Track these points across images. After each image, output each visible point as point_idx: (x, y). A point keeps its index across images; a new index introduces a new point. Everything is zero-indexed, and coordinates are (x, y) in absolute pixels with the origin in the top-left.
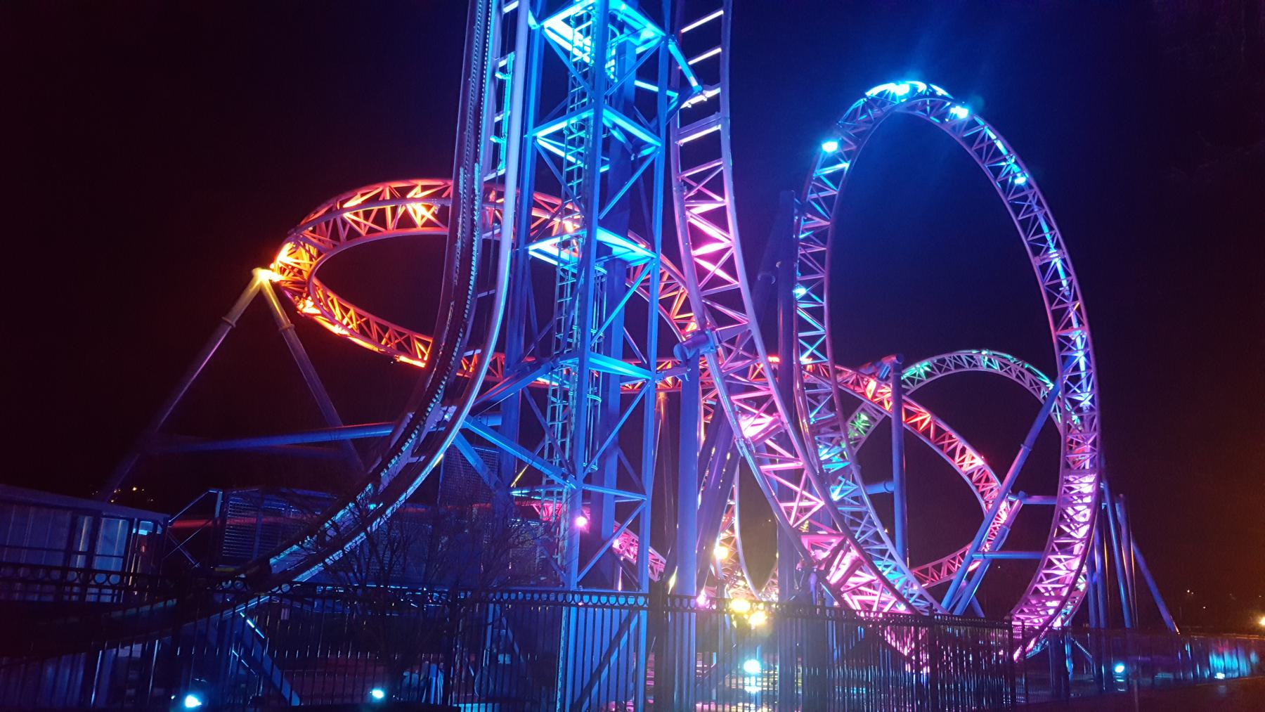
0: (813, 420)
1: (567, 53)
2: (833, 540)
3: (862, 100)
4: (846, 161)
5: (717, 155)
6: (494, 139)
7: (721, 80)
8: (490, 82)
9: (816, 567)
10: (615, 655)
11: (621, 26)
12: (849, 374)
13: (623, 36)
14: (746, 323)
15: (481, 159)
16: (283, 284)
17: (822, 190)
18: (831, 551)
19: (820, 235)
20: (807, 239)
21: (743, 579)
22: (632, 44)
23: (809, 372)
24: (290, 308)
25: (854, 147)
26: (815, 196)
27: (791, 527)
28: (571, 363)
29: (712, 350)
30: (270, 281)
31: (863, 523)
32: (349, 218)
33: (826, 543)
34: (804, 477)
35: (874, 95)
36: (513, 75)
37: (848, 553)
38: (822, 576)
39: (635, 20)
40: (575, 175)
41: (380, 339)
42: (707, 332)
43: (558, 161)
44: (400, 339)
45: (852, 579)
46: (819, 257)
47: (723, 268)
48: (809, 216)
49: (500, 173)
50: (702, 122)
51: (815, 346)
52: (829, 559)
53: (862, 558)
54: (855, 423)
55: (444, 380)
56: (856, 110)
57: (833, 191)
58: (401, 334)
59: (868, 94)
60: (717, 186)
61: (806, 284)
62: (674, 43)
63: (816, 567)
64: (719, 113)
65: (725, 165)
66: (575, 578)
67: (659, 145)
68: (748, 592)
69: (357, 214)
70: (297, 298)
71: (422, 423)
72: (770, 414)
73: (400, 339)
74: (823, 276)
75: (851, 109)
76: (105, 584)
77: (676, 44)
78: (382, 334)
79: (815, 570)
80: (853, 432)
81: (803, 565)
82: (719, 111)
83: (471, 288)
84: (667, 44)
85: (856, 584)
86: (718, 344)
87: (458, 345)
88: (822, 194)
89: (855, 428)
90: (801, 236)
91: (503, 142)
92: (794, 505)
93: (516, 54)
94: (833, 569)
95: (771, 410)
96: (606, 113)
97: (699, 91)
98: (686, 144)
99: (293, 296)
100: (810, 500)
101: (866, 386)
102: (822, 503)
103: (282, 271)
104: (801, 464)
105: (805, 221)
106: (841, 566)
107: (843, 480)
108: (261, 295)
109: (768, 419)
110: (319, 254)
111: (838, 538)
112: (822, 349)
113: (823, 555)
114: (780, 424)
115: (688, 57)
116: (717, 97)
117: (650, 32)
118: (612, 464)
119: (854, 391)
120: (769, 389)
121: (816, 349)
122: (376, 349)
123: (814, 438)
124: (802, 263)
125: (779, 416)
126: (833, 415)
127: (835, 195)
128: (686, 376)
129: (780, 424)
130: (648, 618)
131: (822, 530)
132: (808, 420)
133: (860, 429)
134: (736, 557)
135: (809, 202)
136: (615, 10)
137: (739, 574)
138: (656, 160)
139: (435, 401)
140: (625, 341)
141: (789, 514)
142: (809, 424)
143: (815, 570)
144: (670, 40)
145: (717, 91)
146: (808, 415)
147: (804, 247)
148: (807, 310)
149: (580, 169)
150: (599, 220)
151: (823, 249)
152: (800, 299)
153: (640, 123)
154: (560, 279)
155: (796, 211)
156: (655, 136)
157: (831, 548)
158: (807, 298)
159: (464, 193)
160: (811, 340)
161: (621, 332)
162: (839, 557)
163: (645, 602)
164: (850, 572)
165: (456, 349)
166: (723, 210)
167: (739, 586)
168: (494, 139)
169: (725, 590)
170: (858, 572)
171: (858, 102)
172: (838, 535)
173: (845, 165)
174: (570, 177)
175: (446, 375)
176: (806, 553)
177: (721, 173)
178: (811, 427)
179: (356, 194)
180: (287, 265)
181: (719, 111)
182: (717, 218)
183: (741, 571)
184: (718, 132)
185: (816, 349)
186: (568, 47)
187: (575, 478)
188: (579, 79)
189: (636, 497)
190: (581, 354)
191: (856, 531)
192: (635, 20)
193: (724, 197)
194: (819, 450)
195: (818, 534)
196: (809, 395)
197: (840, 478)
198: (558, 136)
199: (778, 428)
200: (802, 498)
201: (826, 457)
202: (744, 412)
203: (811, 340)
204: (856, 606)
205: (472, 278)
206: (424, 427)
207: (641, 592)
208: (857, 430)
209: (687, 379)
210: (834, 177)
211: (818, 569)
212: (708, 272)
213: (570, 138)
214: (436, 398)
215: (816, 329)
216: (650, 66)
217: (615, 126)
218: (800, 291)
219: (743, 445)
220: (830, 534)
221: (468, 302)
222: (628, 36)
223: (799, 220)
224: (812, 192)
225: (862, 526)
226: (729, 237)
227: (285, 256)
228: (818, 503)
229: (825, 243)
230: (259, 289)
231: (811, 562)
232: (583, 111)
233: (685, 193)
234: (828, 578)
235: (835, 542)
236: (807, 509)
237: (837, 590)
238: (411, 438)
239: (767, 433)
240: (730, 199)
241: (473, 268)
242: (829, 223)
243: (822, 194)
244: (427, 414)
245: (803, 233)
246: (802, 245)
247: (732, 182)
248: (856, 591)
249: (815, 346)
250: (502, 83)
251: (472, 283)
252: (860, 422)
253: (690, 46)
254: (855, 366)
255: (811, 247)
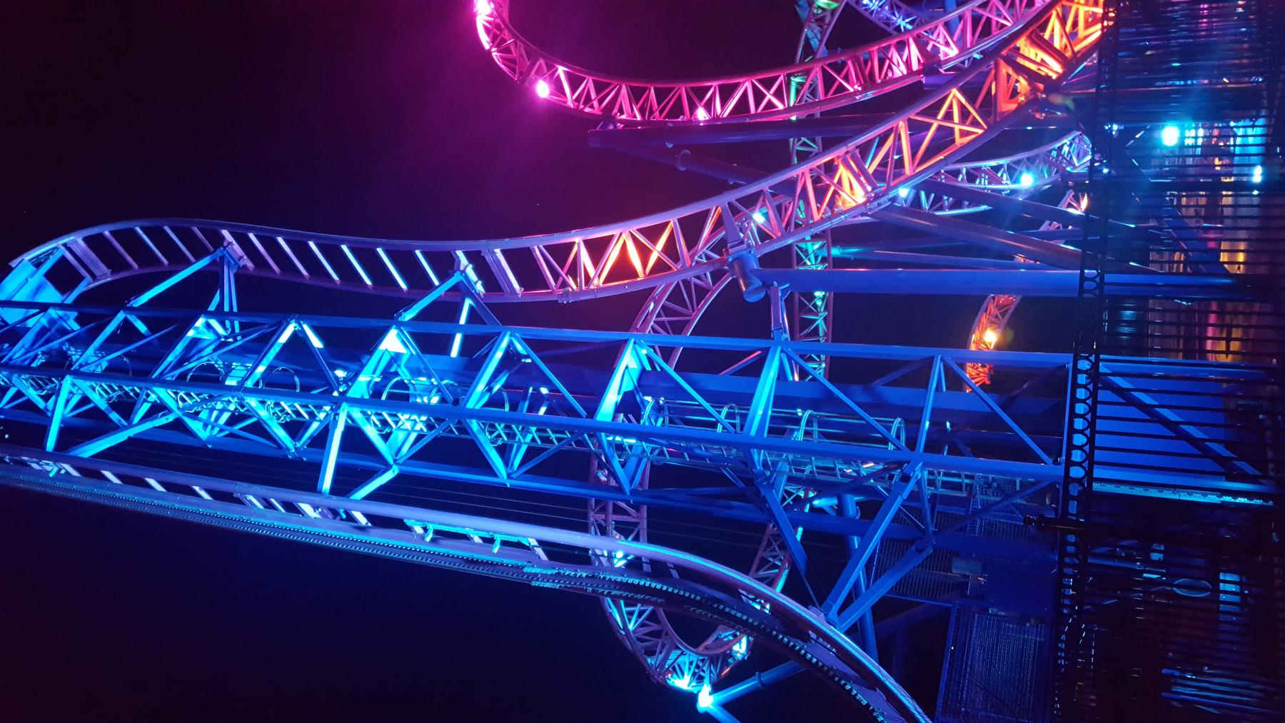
0: (856, 87)
1: (420, 437)
2: (1004, 71)
3: (493, 54)
4: (557, 70)
5: (528, 252)
6: (496, 548)
7: (447, 250)
8: (440, 546)
9: (1039, 94)
10: (1166, 413)
11: (387, 374)
12: (811, 33)
13: (399, 371)
14: (719, 208)
15: (520, 563)
16: (714, 677)
17: (588, 94)
18: (1018, 74)
19: (636, 95)
20: (642, 111)
21: (1060, 148)
22: (409, 360)
23: (806, 80)
24: (741, 671)
25: (542, 61)
26: (596, 104)
27: (986, 132)
28: (758, 457)
29: (752, 253)
30: (711, 694)
31: (986, 14)
32: (636, 622)
33: (1008, 82)
34: (919, 118)
35: (488, 40)
36: (428, 522)
37: (1021, 52)
38: (1052, 86)
39: (379, 362)
40: (544, 435)
41: (775, 566)
42: (730, 260)
43: (532, 452)
44: (775, 545)
45: (1057, 44)
46: (661, 95)
47: (654, 240)
48: (615, 110)
49: (535, 543)
50: (494, 268)
51: (766, 92)
52: (1029, 77)
53: (1028, 33)
54: (873, 11)
55: (777, 636)
56: (504, 59)
57: (588, 84)
58: (769, 544)
59: (487, 47)
60: (562, 252)
61: (693, 108)
62: (404, 314)
63: (1039, 94)
64: (483, 251)
65: (538, 245)
66: (1048, 469)
67: (509, 333)
68: (1077, 140)
69: (630, 614)
70: (730, 660)
71: (831, 673)
72: (836, 169)
73: (775, 545)
74: (683, 89)
75: (502, 66)
76: (1093, 361)
77: (405, 311)
78: (771, 564)
79: (1044, 96)
80: (884, 13)
81: (1038, 111)
82: (480, 252)
83: (665, 588)
84: (404, 324)
85: (1062, 36)
86: (745, 246)
87: (733, 612)
88: (593, 95)
89: (879, 9)
90: (639, 118)
91: (498, 538)
92: (957, 128)
93: (405, 518)
94: (1044, 71)
95: (830, 168)
96: (470, 405)
97: (461, 275)
98: (521, 284)
99: (728, 664)
100: (951, 107)
101: (824, 9)
102: (955, 92)
103: (700, 679)
104: (901, 124)
105: (622, 113)
106: (1038, 60)
107: (931, 44)
108: (727, 706)
109: (843, 172)
110: (677, 648)
111: (1001, 66)
112: (768, 84)
113: (1023, 84)
114: (848, 156)
115: (430, 287)
116: (467, 254)
117: (393, 342)
118: (895, 395)
119: (829, 24)
120: (803, 174)
121: (768, 89)
122: (786, 572)
123: (879, 84)
124: (668, 116)
125: (838, 157)
126: (850, 63)
127: (593, 80)
128: (782, 288)
129: (848, 156)
130: (1113, 272)
131: (990, 88)
132: (856, 92)
133: (880, 4)
134: (1031, 160)
135: (601, 111)
136: (368, 386)
137: (1054, 153)
138: (525, 337)
139: (803, 652)
140: (739, 373)
141: (969, 133)
142: (860, 93)
143: (1044, 96)
144: (400, 319)
145: (460, 254)
146: (851, 93)
147: (651, 112)
148: (724, 103)
149: (537, 430)
150: (587, 417)
151: (652, 90)
152: (710, 113)
153: (487, 354)
154: (661, 455)
155: (611, 127)
156: (500, 339)
157: (1014, 76)
158: (709, 106)
159: (559, 582)
160: (759, 97)
161: (723, 381)
162: (1027, 64)
163: (1087, 358)
164: (1047, 47)
165: (739, 615)
166: (588, 243)
167: (1069, 152)
168: (496, 548)
169: (1075, 171)
170: (1047, 36)
171: (495, 57)
172: (997, 67)
173: (561, 70)
174: (546, 440)
175: (771, 632)
176: (1021, 107)
177: (545, 247)
178: (865, 90)
179: (610, 613)
180: (694, 674)
181: (480, 252)
182: (597, 249)
183: (1050, 151)
184: (504, 252)
185: (768, 89)
186: (413, 436)
187: (908, 462)
188: (444, 425)
189: (938, 367)
190: (747, 447)
191: (997, 22)
192: (379, 362)
193: (574, 243)
194: (896, 76)
195: (996, 94)
196: (826, 93)
197: (929, 48)
198: (504, 451)
199: (853, 158)
200: (949, 116)
201: (903, 68)
202: (832, 204)
203: (759, 97)
204: (1096, 32)
205: (653, 585)
206: (837, 670)
207: (1070, 366)
208: (881, 7)
209: (787, 286)
210: (575, 82)
211: (1043, 92)
212: (659, 259)
213: (505, 439)
214: (800, 649)
215: (745, 92)
216: (431, 343)
217: (490, 385)
218: (701, 114)
219: (875, 203)
220: (996, 78)
221: (682, 593)
222: (399, 366)
223: (622, 121)
224: (592, 107)
225: (990, 16)
226: (618, 235)
227: (682, 683)
228: (954, 96)
229: (646, 89)
230: (721, 708)
231: (1033, 102)
232: (472, 430)
233: (570, 290)
234: (1054, 76)
235: (1005, 69)
236: (962, 109)
237: (1069, 63)
238: (851, 690)
239: (860, 173)
240: (576, 235)
241: (642, 583)
242: (624, 86)
243: (593, 95)
244: (821, 664)
245: (635, 116)
246: (649, 116)
247: (556, 234)
248: (1072, 36)
249: (766, 92)
250: (437, 532)
251: (659, 586)
252: (871, 5)
253: (420, 284)
254: (797, 26)
255: (651, 105)
